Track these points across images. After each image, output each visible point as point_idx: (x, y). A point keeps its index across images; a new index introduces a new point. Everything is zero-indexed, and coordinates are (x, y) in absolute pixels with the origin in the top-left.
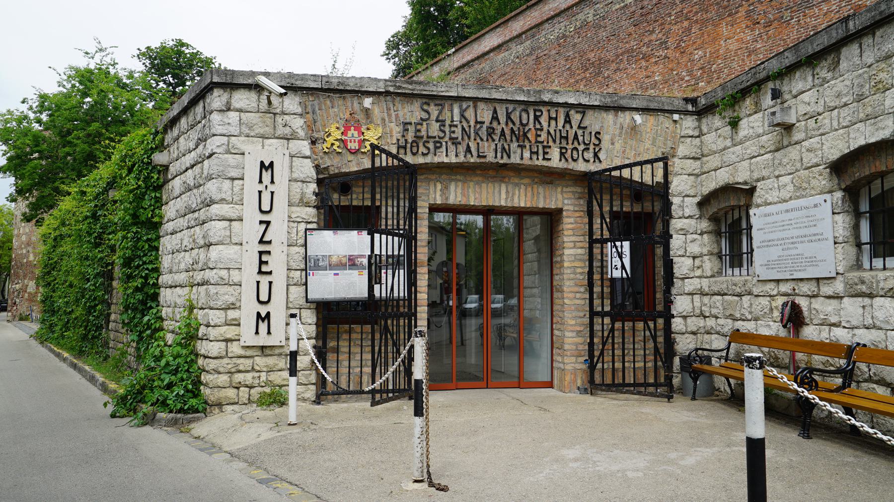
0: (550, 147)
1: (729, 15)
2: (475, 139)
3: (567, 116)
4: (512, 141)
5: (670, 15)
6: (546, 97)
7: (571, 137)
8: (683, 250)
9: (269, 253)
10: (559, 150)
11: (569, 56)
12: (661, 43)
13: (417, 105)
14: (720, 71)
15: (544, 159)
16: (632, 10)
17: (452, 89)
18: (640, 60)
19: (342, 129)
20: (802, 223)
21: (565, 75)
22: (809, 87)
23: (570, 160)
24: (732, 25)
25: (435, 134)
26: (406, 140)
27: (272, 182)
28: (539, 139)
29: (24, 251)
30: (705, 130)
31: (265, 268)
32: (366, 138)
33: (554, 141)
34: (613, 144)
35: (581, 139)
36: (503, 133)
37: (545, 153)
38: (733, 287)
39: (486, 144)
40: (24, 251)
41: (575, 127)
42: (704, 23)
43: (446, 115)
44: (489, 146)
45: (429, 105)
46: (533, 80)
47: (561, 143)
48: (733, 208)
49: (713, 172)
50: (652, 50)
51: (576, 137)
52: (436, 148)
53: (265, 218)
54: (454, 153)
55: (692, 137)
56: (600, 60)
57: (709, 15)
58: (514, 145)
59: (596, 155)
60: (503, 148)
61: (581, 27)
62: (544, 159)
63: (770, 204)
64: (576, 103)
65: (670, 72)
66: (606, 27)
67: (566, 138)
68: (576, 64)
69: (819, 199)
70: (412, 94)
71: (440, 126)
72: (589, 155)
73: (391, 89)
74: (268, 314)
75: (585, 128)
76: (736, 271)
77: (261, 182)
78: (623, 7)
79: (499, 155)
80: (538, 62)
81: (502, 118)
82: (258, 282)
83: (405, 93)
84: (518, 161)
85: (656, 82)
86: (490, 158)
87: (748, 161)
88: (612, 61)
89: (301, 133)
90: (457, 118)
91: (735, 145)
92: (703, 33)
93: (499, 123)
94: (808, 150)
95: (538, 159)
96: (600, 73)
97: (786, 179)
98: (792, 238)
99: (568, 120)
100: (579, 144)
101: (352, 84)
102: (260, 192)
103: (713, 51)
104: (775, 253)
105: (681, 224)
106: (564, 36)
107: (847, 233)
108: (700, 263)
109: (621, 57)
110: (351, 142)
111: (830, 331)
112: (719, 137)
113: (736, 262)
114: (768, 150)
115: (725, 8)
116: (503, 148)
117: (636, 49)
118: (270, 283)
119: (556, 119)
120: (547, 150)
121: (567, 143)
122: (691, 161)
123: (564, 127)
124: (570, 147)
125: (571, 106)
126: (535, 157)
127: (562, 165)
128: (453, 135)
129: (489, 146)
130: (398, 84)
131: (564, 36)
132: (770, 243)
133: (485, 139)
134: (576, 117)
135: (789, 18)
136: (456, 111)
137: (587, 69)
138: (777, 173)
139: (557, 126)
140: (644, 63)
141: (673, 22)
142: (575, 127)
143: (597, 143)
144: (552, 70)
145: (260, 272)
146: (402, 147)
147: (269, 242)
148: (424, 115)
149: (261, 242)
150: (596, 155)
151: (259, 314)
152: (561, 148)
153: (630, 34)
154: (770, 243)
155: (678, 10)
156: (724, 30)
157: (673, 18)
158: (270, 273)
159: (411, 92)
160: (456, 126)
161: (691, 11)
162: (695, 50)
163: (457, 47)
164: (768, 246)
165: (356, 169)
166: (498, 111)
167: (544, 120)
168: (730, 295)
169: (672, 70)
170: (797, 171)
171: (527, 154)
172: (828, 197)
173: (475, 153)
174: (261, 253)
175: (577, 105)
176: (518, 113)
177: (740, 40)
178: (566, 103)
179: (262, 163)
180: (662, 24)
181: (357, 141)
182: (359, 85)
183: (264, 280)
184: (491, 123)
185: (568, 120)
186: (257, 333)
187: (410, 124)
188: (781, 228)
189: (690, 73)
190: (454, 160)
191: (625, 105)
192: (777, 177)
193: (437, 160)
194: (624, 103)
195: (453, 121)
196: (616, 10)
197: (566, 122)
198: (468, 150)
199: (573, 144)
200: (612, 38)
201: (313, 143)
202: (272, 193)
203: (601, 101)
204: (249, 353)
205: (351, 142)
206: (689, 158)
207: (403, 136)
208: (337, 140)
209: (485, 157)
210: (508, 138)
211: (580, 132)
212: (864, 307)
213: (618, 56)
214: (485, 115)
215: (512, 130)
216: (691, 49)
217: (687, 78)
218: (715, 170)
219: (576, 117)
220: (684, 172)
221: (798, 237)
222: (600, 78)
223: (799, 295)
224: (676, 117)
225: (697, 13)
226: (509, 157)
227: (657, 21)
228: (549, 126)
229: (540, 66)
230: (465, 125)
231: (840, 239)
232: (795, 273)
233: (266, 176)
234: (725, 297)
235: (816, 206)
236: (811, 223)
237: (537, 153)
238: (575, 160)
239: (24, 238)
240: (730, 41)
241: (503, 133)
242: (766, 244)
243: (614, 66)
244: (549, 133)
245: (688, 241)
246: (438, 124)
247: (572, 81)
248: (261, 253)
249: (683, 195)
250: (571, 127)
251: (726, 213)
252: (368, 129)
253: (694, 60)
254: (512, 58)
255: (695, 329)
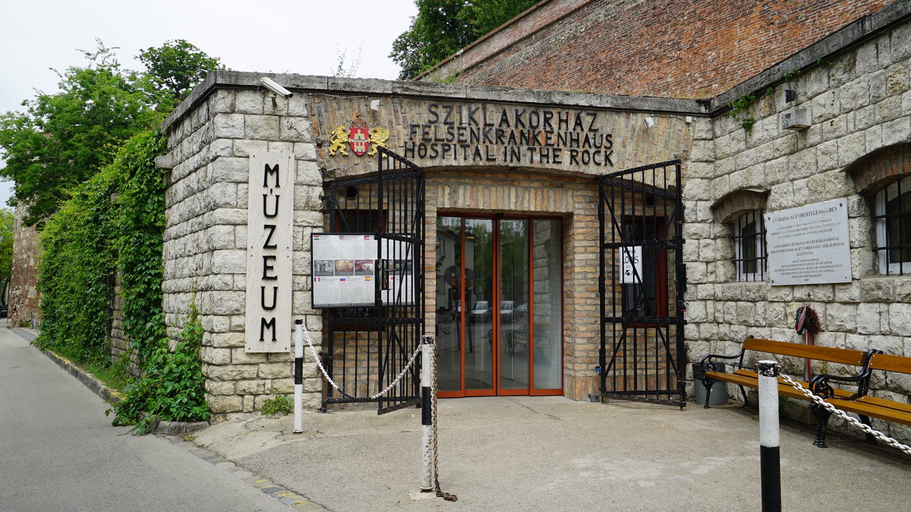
0: (560, 150)
1: (743, 16)
2: (484, 142)
3: (578, 118)
4: (521, 143)
5: (682, 15)
6: (557, 99)
7: (582, 140)
8: (696, 255)
9: (274, 258)
10: (569, 153)
11: (580, 57)
12: (674, 44)
13: (424, 107)
14: (734, 72)
15: (554, 162)
16: (644, 10)
17: (461, 91)
18: (652, 61)
19: (349, 132)
20: (817, 227)
21: (576, 77)
22: (824, 89)
23: (581, 163)
24: (746, 26)
25: (444, 137)
26: (414, 143)
27: (278, 186)
28: (549, 142)
29: (25, 256)
30: (718, 133)
31: (270, 274)
32: (373, 140)
33: (565, 144)
34: (624, 147)
35: (592, 141)
36: (512, 136)
37: (555, 156)
38: (747, 293)
39: (495, 147)
40: (25, 256)
41: (586, 130)
42: (717, 23)
43: (455, 117)
44: (498, 149)
45: (437, 107)
46: (543, 82)
47: (571, 146)
48: (747, 212)
49: (727, 176)
50: (665, 51)
51: (587, 140)
52: (444, 151)
53: (270, 222)
54: (463, 156)
55: (705, 139)
56: (611, 61)
57: (723, 15)
58: (524, 148)
59: (607, 158)
60: (513, 151)
61: (592, 27)
62: (554, 162)
63: (785, 208)
64: (587, 105)
65: (683, 73)
66: (617, 27)
67: (577, 141)
68: (587, 65)
69: (835, 203)
70: (420, 96)
71: (448, 129)
72: (600, 158)
73: (399, 91)
74: (273, 320)
75: (596, 130)
76: (750, 276)
77: (266, 185)
78: (635, 7)
79: (508, 158)
80: (548, 64)
81: (512, 121)
82: (263, 288)
83: (413, 95)
84: (528, 164)
85: (668, 84)
86: (500, 161)
87: (763, 164)
88: (624, 63)
89: (307, 136)
90: (465, 120)
91: (749, 148)
92: (716, 34)
93: (509, 126)
94: (823, 153)
95: (548, 162)
96: (611, 74)
97: (801, 183)
98: (807, 242)
99: (579, 123)
100: (590, 147)
101: (358, 86)
102: (265, 196)
103: (726, 52)
104: (789, 258)
105: (694, 228)
106: (575, 37)
107: (863, 238)
108: (714, 269)
109: (633, 58)
110: (357, 145)
111: (846, 337)
112: (733, 139)
113: (750, 267)
114: (783, 153)
115: (739, 8)
116: (513, 151)
117: (649, 50)
118: (276, 289)
119: (566, 121)
120: (558, 153)
121: (578, 146)
122: (705, 164)
123: (574, 129)
124: (581, 149)
125: (582, 108)
126: (545, 160)
127: (573, 168)
128: (462, 138)
129: (498, 149)
130: (405, 86)
131: (575, 37)
132: (785, 248)
133: (494, 142)
134: (587, 120)
135: (804, 19)
136: (465, 113)
137: (599, 71)
138: (791, 177)
139: (567, 129)
140: (656, 65)
141: (686, 22)
142: (586, 130)
143: (608, 145)
144: (563, 72)
145: (265, 278)
146: (410, 150)
147: (275, 247)
148: (432, 118)
149: (266, 246)
150: (607, 158)
151: (263, 320)
152: (572, 151)
153: (642, 35)
154: (785, 248)
155: (691, 10)
156: (738, 30)
157: (685, 18)
158: (275, 278)
159: (419, 94)
160: (465, 129)
161: (704, 11)
162: (709, 51)
163: (466, 48)
164: (782, 251)
165: (363, 172)
166: (508, 114)
167: (554, 123)
168: (744, 301)
169: (685, 71)
170: (812, 174)
171: (537, 158)
172: (843, 201)
173: (484, 156)
174: (266, 258)
175: (588, 107)
176: (528, 116)
177: (754, 41)
178: (577, 105)
179: (267, 166)
180: (675, 25)
181: (363, 144)
182: (365, 87)
183: (269, 286)
184: (500, 125)
185: (579, 123)
186: (262, 339)
187: (418, 126)
188: (796, 233)
189: (703, 74)
190: (462, 163)
191: (637, 107)
192: (792, 180)
193: (445, 163)
194: (635, 105)
195: (461, 123)
196: (628, 10)
197: (576, 124)
198: (477, 153)
199: (584, 147)
200: (623, 38)
201: (319, 145)
202: (277, 197)
203: (612, 103)
204: (254, 360)
205: (357, 145)
206: (702, 161)
207: (411, 139)
208: (343, 143)
209: (494, 160)
210: (518, 140)
211: (591, 135)
212: (880, 313)
213: (629, 57)
214: (495, 117)
215: (522, 133)
216: (704, 50)
217: (700, 80)
218: (729, 173)
219: (587, 120)
220: (697, 175)
221: (813, 242)
222: (611, 80)
223: (814, 301)
224: (689, 119)
225: (710, 13)
226: (519, 160)
227: (670, 21)
228: (560, 128)
229: (550, 68)
230: (474, 127)
231: (856, 244)
232: (810, 278)
233: (271, 180)
234: (739, 303)
235: (831, 210)
236: (827, 228)
237: (547, 156)
238: (585, 164)
239: (24, 243)
240: (743, 42)
241: (512, 136)
242: (781, 248)
243: (625, 67)
244: (559, 135)
245: (701, 246)
246: (447, 127)
247: (583, 82)
248: (266, 258)
249: (696, 199)
250: (582, 130)
251: (740, 218)
252: (375, 132)
253: (707, 62)
254: (522, 59)
255: (708, 335)
